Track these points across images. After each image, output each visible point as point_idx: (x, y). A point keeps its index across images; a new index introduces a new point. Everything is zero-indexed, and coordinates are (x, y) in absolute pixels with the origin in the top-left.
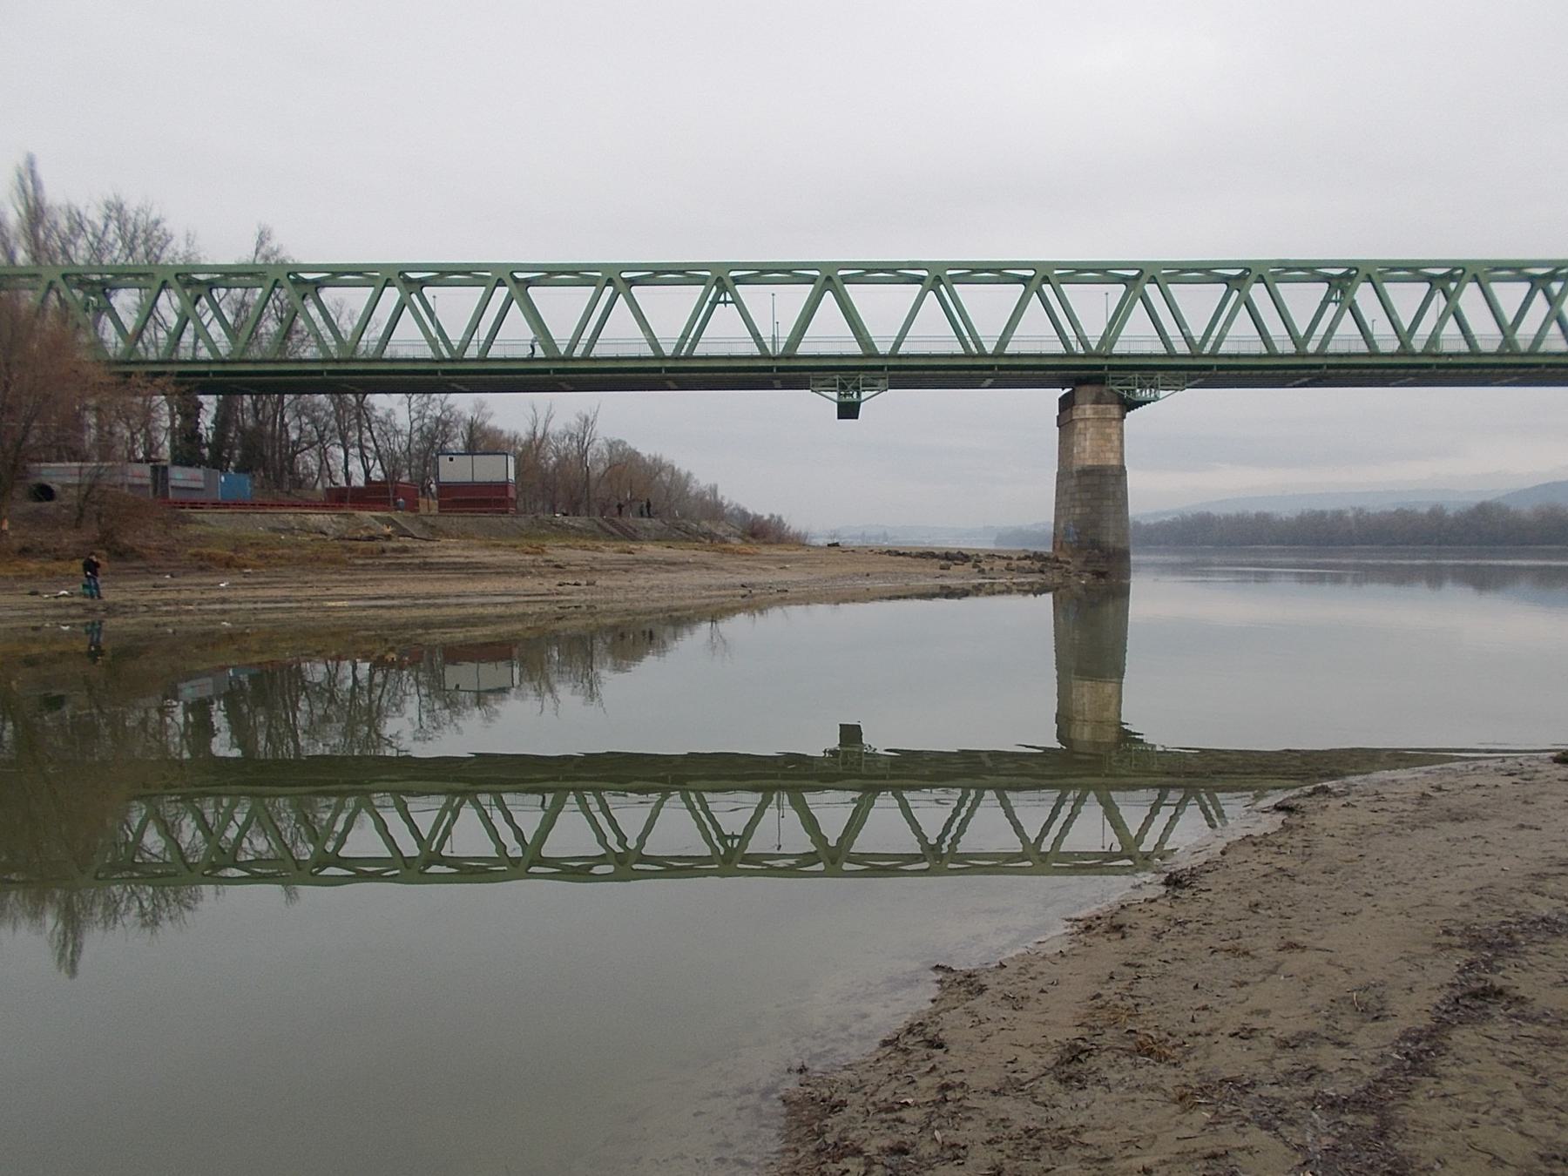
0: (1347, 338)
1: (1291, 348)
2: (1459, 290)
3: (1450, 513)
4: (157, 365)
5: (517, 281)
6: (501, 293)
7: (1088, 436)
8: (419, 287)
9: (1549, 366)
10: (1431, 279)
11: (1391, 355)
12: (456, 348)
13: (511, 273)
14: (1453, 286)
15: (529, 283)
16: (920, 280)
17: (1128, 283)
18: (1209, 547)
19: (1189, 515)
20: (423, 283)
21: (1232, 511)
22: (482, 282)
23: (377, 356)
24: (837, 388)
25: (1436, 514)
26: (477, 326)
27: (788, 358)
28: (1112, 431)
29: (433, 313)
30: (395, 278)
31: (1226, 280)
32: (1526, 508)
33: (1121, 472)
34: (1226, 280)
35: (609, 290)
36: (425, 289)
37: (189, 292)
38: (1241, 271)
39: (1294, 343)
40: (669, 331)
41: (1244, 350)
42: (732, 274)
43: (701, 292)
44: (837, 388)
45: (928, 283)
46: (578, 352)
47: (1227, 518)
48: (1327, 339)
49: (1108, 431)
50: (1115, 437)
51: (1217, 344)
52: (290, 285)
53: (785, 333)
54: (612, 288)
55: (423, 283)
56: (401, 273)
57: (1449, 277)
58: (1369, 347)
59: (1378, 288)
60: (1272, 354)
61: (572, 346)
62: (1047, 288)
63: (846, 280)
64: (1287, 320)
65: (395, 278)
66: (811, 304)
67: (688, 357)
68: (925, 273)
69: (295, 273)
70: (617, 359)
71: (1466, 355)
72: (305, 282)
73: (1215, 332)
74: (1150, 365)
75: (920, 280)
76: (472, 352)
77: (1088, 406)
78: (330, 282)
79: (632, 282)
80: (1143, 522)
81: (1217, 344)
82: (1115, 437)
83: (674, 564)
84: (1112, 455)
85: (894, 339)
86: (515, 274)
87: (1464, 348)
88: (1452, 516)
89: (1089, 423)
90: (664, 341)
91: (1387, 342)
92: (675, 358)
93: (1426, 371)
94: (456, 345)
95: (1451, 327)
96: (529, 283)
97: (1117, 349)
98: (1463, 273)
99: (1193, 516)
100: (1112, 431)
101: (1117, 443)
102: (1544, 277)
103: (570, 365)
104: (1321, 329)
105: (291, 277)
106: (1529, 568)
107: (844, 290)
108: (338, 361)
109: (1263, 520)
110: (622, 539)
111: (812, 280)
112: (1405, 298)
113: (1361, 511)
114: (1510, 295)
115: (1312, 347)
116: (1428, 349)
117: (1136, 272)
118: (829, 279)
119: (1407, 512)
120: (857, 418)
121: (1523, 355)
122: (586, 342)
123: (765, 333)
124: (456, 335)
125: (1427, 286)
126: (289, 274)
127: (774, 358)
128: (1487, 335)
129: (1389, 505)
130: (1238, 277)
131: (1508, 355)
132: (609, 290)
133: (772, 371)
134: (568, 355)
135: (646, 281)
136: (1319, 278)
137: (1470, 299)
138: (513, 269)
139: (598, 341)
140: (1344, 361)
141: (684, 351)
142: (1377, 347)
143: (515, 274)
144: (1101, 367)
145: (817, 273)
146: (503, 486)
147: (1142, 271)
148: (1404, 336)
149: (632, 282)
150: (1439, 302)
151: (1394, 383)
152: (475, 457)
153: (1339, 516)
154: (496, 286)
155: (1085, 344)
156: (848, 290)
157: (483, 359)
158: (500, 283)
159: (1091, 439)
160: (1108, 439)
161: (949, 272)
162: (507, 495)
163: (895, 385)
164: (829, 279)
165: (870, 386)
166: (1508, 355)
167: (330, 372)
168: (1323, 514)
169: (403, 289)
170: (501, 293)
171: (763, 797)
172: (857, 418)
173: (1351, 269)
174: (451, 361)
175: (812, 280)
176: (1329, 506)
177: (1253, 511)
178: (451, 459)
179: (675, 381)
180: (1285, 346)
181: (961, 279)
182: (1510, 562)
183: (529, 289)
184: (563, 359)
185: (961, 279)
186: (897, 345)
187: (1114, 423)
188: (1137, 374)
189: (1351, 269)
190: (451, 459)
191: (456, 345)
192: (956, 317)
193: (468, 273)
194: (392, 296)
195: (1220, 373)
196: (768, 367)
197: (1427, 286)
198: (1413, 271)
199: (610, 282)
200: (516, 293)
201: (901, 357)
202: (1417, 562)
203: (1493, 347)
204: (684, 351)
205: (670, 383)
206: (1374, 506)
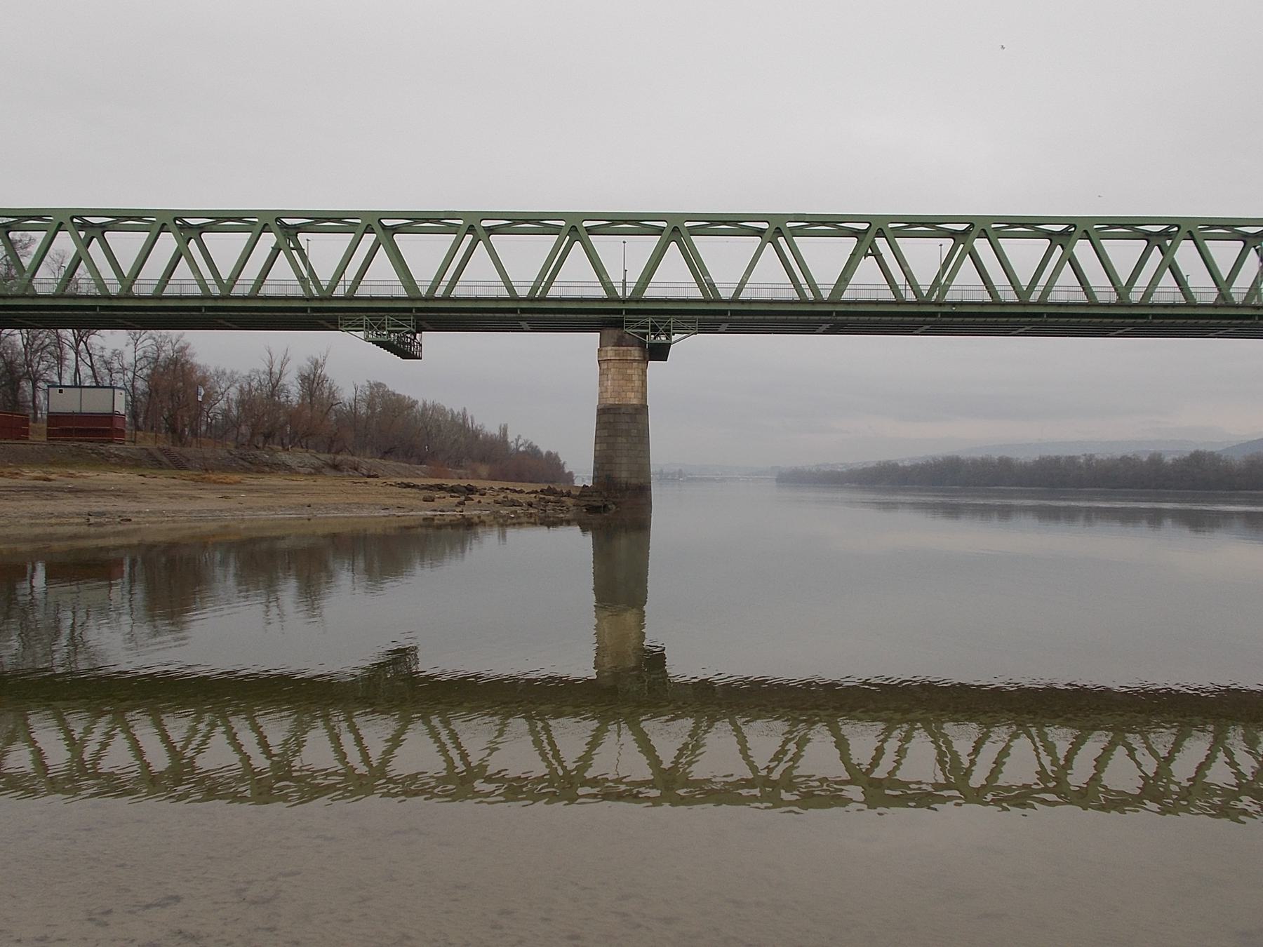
0: (1066, 290)
1: (1114, 298)
2: (1174, 247)
3: (1168, 459)
4: (575, 303)
5: (384, 227)
6: (369, 239)
7: (610, 376)
8: (392, 233)
9: (1155, 316)
10: (1147, 236)
11: (1109, 305)
12: (325, 288)
13: (379, 220)
14: (1169, 242)
15: (395, 230)
16: (759, 233)
17: (1150, 238)
18: (957, 487)
19: (940, 459)
20: (202, 229)
21: (978, 455)
22: (351, 228)
23: (253, 294)
24: (364, 328)
25: (1156, 461)
26: (344, 272)
27: (638, 301)
28: (634, 371)
29: (306, 257)
30: (272, 223)
31: (1049, 235)
32: (1238, 459)
33: (643, 409)
34: (1049, 235)
35: (469, 238)
36: (106, 234)
37: (82, 234)
38: (1066, 226)
39: (1016, 292)
40: (524, 276)
41: (967, 297)
42: (586, 224)
43: (147, 236)
44: (364, 328)
45: (768, 235)
46: (440, 292)
47: (974, 462)
48: (1150, 290)
49: (629, 371)
50: (635, 378)
51: (1046, 291)
52: (177, 230)
53: (634, 277)
54: (472, 236)
55: (202, 229)
56: (278, 219)
57: (1166, 234)
58: (1019, 297)
59: (1200, 245)
60: (1093, 303)
61: (434, 287)
62: (781, 240)
63: (694, 231)
64: (1078, 273)
65: (272, 223)
66: (391, 250)
67: (540, 300)
68: (664, 224)
69: (180, 219)
70: (477, 299)
71: (797, 302)
72: (191, 227)
73: (448, 276)
74: (1111, 314)
75: (759, 233)
76: (340, 291)
77: (609, 348)
78: (16, 226)
79: (491, 231)
80: (900, 465)
81: (1046, 291)
82: (635, 378)
83: (82, 491)
84: (632, 395)
85: (430, 283)
86: (382, 221)
87: (1180, 299)
88: (1171, 462)
89: (611, 364)
90: (1098, 289)
91: (1104, 292)
92: (529, 299)
93: (1249, 322)
94: (325, 285)
95: (1168, 279)
96: (395, 230)
97: (949, 297)
98: (1178, 231)
99: (943, 458)
100: (634, 371)
101: (637, 383)
102: (101, 225)
103: (431, 305)
104: (1043, 281)
105: (177, 222)
106: (1238, 513)
107: (1205, 244)
108: (216, 298)
109: (1006, 464)
110: (169, 468)
111: (659, 231)
112: (1124, 253)
113: (1091, 456)
114: (1224, 252)
115: (1135, 297)
116: (1246, 302)
117: (965, 226)
118: (676, 229)
119: (1130, 458)
120: (666, 360)
121: (1237, 306)
122: (447, 284)
123: (615, 277)
124: (325, 274)
125: (1241, 244)
126: (72, 218)
127: (624, 301)
128: (1203, 287)
129: (1118, 453)
130: (1060, 233)
131: (1222, 306)
132: (469, 238)
133: (306, 311)
134: (430, 295)
135: (405, 229)
136: (1236, 236)
137: (1186, 253)
138: (278, 216)
139: (266, 282)
140: (1062, 310)
141: (935, 297)
142: (1095, 298)
143: (382, 221)
144: (619, 311)
145: (664, 224)
146: (111, 417)
147: (972, 225)
148: (1122, 291)
149: (491, 231)
150: (1156, 256)
151: (1211, 335)
152: (83, 389)
153: (1072, 460)
154: (262, 231)
155: (917, 291)
156: (1103, 244)
157: (349, 298)
158: (369, 230)
159: (613, 379)
160: (629, 379)
161: (687, 224)
162: (112, 425)
163: (704, 330)
164: (676, 229)
165: (680, 329)
166: (1222, 306)
167: (209, 309)
168: (1058, 459)
169: (280, 235)
170: (369, 239)
171: (1140, 793)
172: (666, 360)
173: (1071, 225)
174: (321, 299)
175: (659, 231)
176: (1063, 452)
177: (996, 456)
178: (61, 391)
179: (229, 320)
180: (1009, 295)
181: (700, 231)
182: (1063, 504)
183: (203, 235)
184: (426, 299)
185: (700, 231)
186: (739, 291)
187: (635, 364)
188: (649, 319)
189: (1172, 226)
190: (61, 391)
191: (325, 285)
192: (794, 267)
193: (239, 219)
194: (268, 241)
195: (1155, 321)
196: (1252, 315)
197: (1241, 244)
198: (1129, 227)
199: (471, 230)
200: (383, 239)
201: (743, 302)
202: (991, 502)
203: (1212, 298)
204: (935, 297)
205: (524, 324)
206: (1102, 454)
